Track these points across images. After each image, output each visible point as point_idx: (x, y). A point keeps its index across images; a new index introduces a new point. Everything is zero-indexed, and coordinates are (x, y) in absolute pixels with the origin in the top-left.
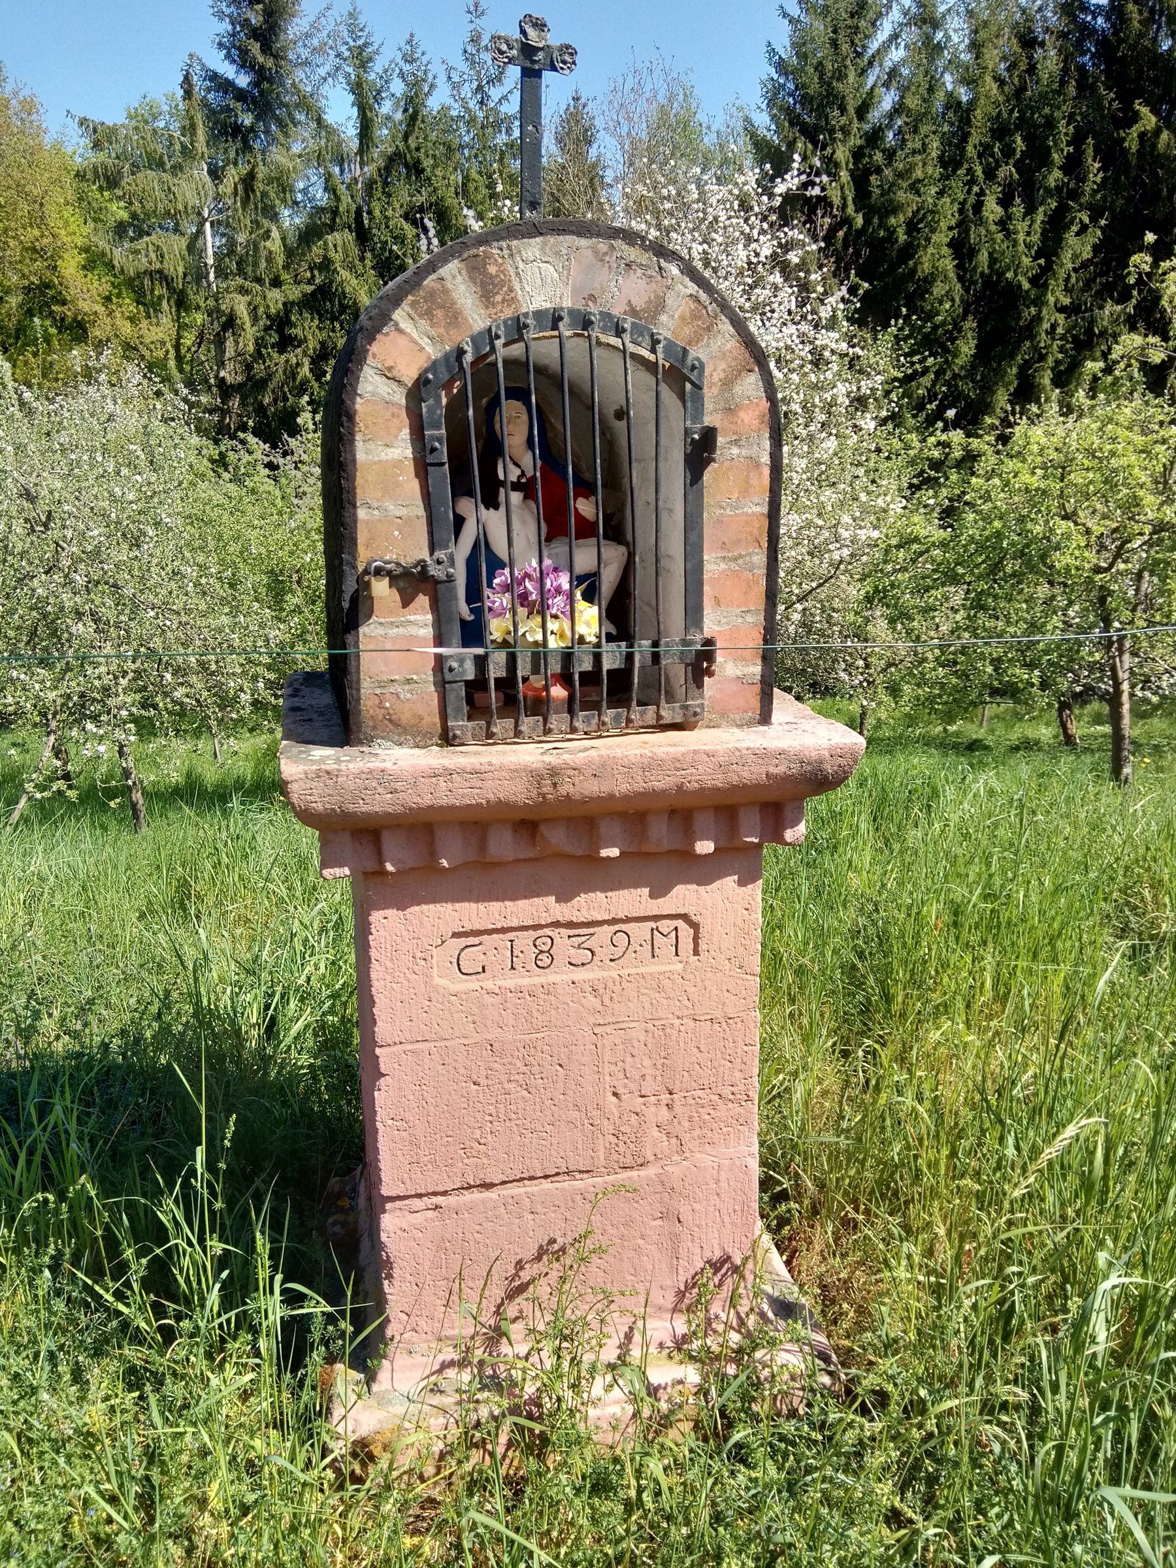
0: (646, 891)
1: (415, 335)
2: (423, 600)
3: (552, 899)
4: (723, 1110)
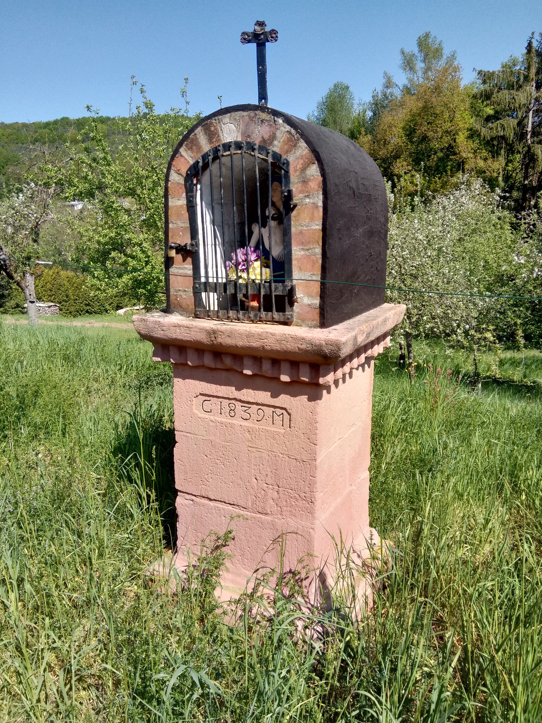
0: (269, 394)
1: (186, 157)
2: (189, 260)
3: (234, 388)
4: (301, 503)
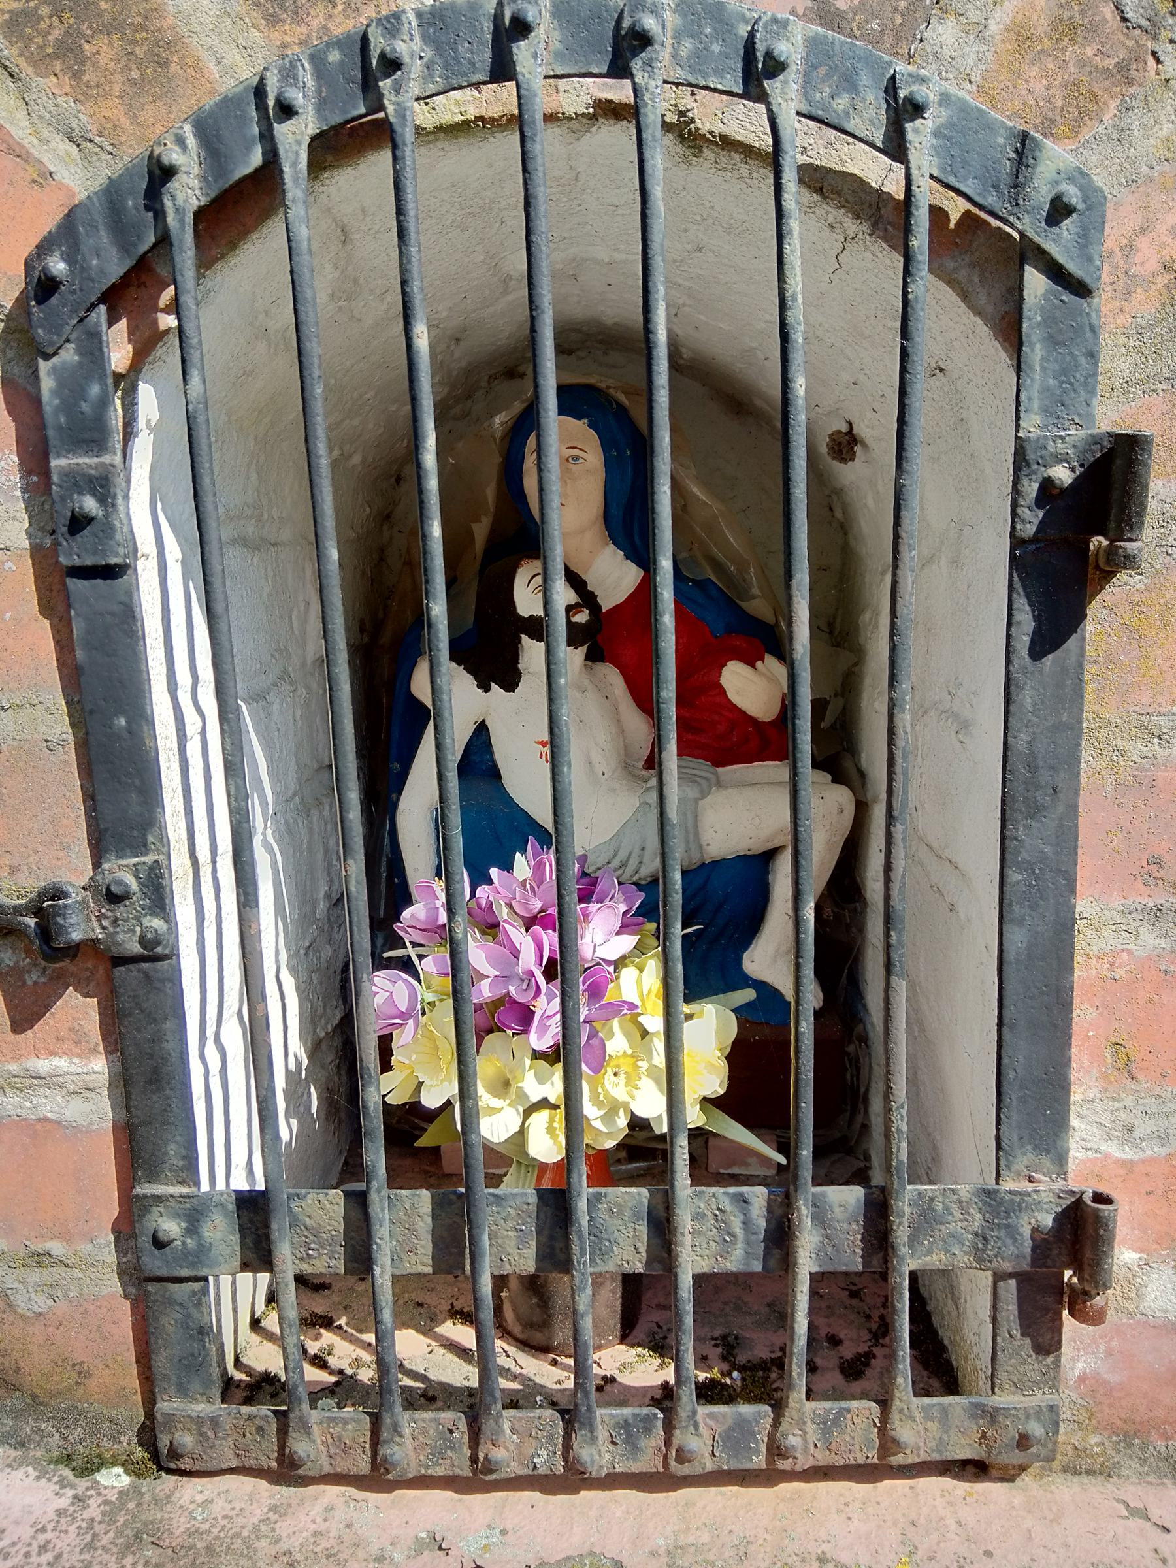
2: (78, 1010)
